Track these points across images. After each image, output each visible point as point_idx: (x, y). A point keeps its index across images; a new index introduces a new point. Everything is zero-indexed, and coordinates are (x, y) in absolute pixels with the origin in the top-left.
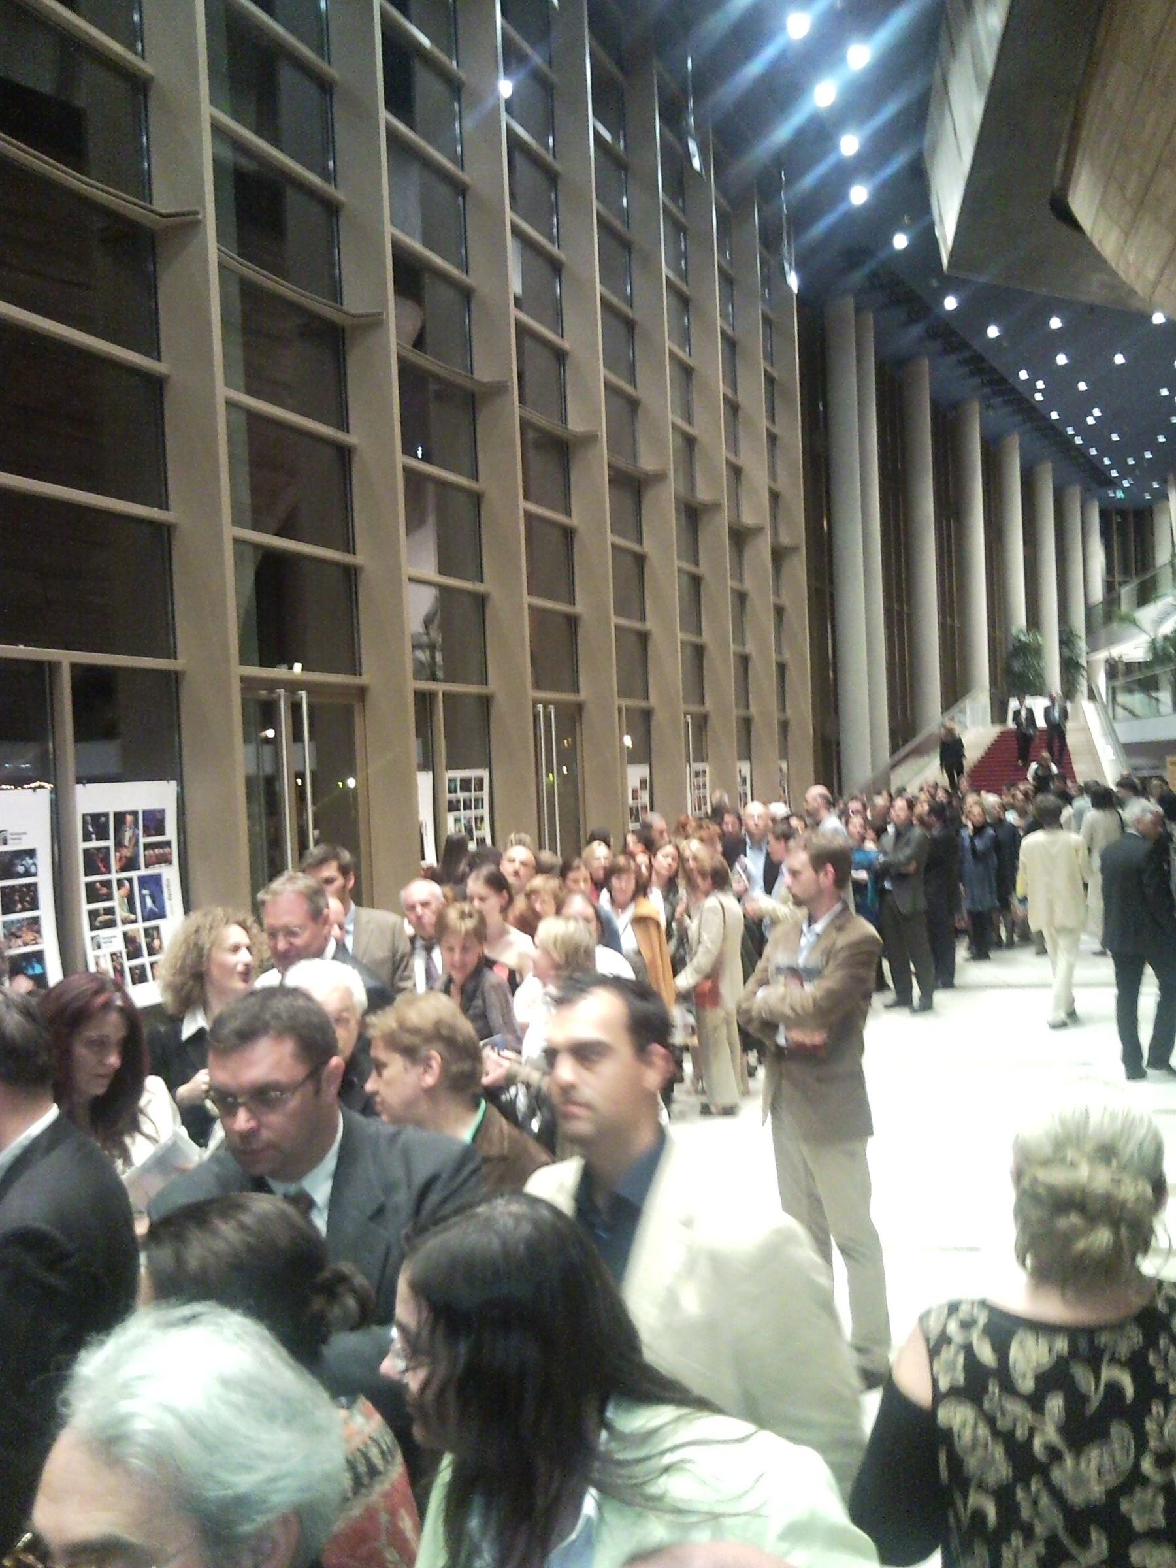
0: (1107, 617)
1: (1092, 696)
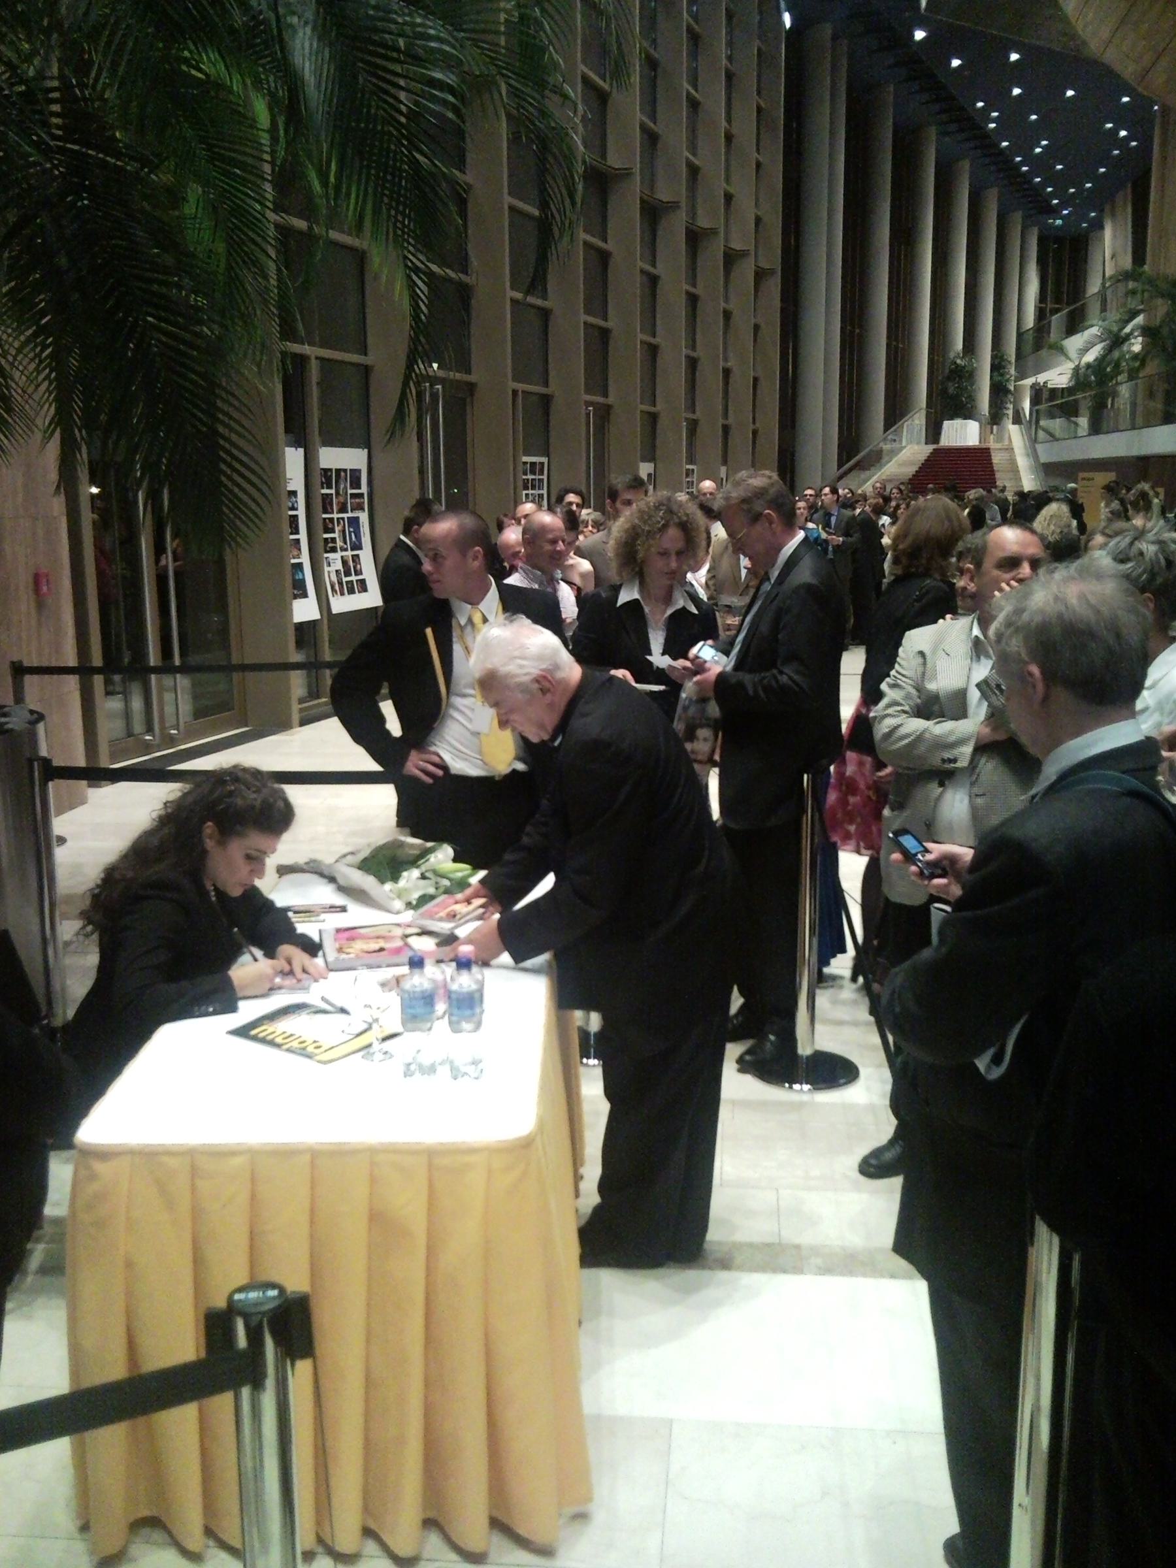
0: (1039, 344)
1: (1017, 420)
